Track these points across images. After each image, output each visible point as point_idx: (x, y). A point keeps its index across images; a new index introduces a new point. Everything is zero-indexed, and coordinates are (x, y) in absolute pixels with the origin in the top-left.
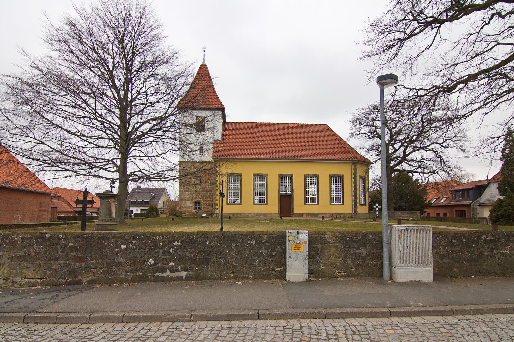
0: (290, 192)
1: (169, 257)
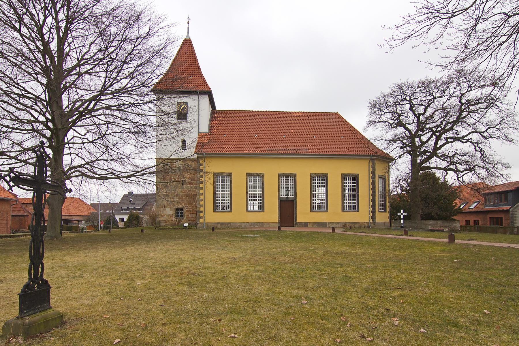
0: (293, 196)
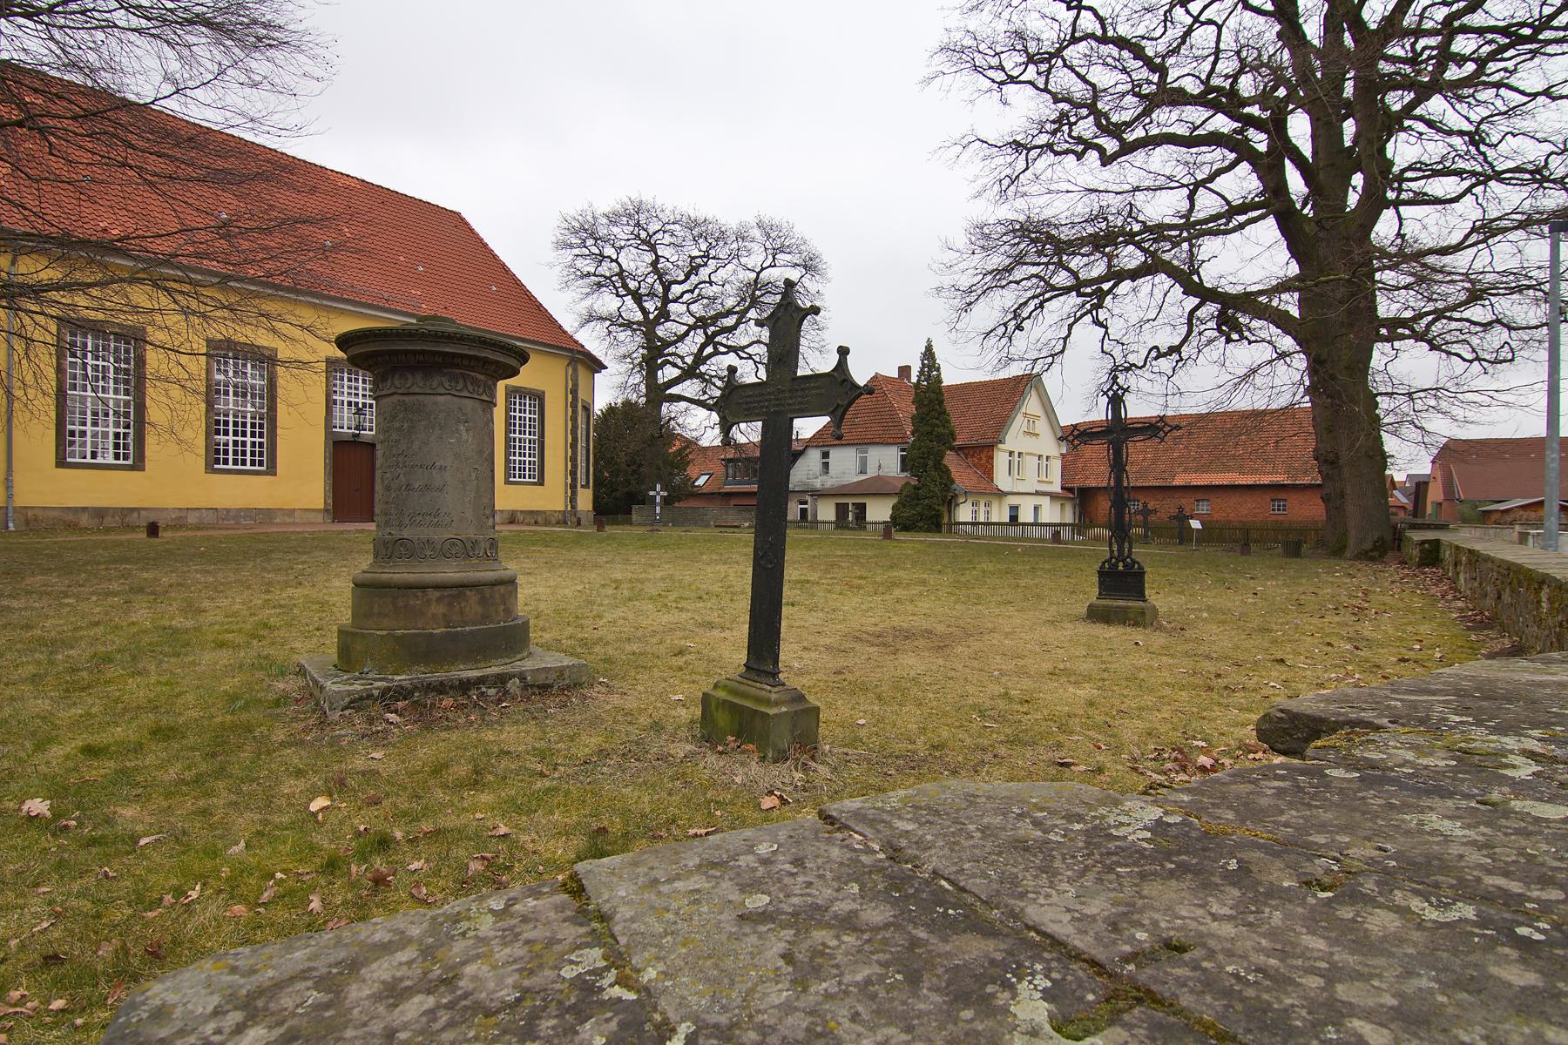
0: (371, 430)
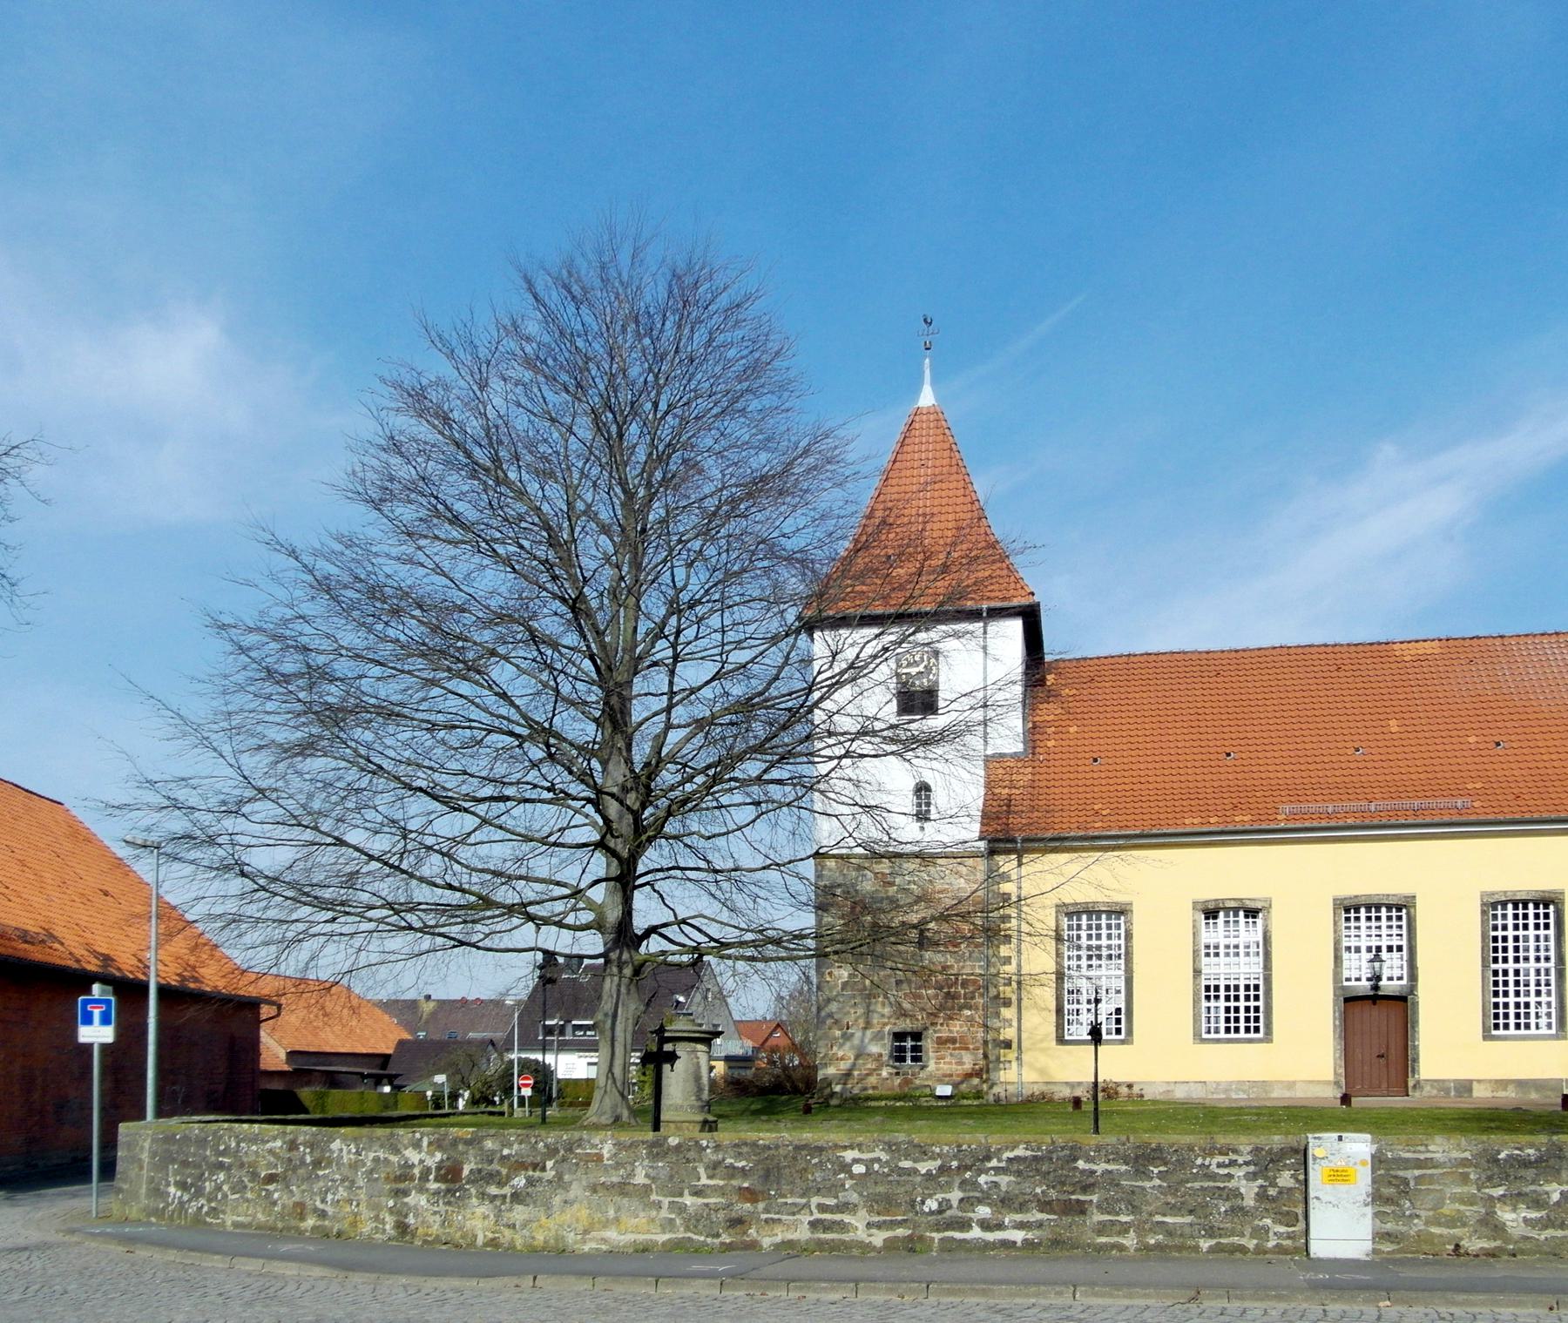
0: (1400, 978)
1: (977, 1194)
